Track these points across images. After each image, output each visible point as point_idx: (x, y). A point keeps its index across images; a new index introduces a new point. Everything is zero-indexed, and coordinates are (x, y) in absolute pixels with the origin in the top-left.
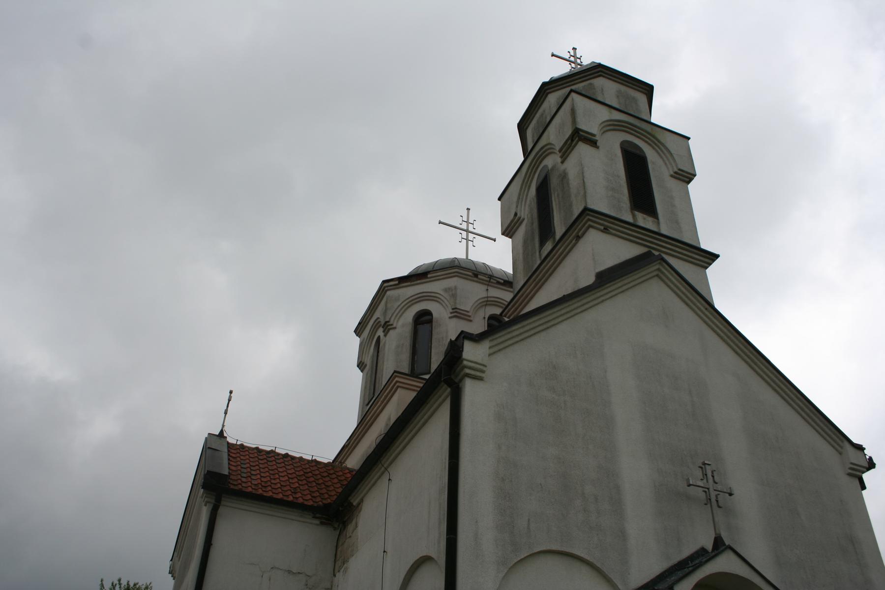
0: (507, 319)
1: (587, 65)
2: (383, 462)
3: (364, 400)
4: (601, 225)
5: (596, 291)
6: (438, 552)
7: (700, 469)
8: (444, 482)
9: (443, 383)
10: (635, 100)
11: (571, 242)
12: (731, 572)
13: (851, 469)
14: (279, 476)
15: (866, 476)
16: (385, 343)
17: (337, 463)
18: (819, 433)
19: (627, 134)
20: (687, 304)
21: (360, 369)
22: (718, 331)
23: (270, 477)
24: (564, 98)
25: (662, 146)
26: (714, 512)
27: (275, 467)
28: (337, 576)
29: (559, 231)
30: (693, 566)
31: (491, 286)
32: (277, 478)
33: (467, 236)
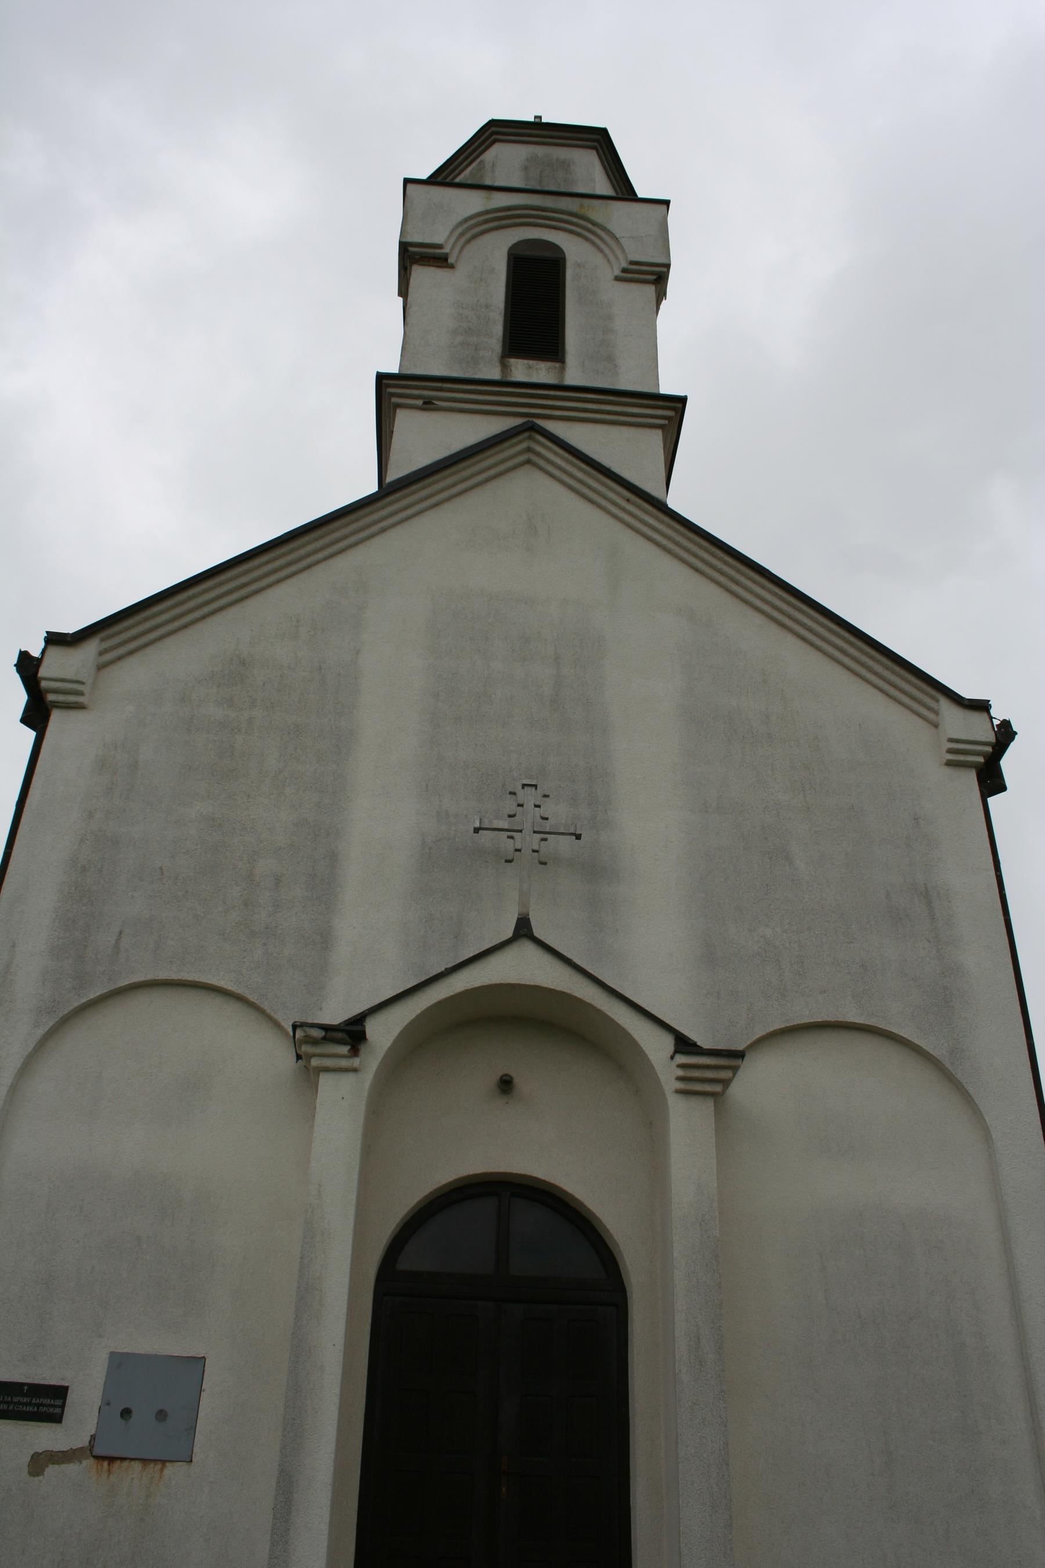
4: (418, 397)
12: (523, 982)
13: (950, 751)
19: (526, 229)
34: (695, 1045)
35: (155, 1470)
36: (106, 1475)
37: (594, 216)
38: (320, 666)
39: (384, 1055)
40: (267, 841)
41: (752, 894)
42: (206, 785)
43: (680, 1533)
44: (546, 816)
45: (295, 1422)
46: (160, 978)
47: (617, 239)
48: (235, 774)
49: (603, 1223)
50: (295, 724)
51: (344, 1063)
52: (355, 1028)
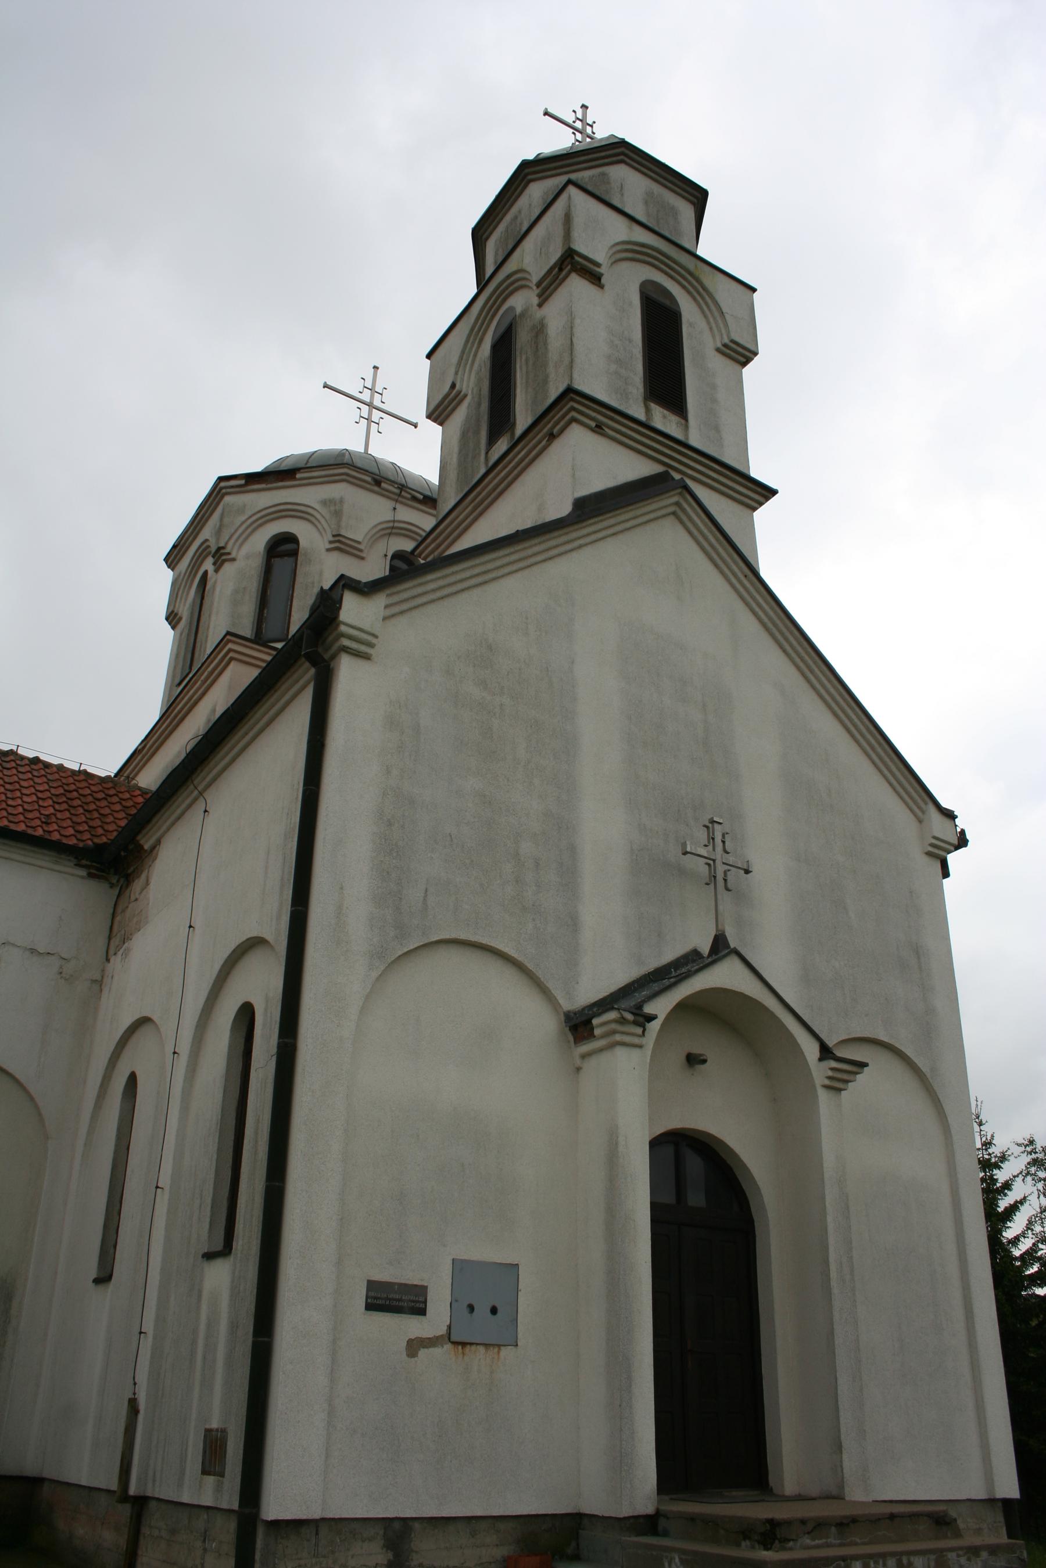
0: (422, 562)
1: (601, 140)
2: (196, 782)
3: (174, 676)
5: (571, 528)
6: (278, 934)
7: (705, 829)
8: (292, 822)
9: (303, 659)
10: (674, 212)
11: (540, 442)
13: (932, 845)
14: (22, 794)
15: (953, 859)
16: (215, 582)
17: (122, 778)
18: (894, 789)
19: (653, 270)
20: (716, 566)
21: (170, 624)
22: (760, 613)
23: (5, 794)
24: (555, 193)
25: (708, 295)
26: (719, 897)
27: (16, 778)
28: (111, 960)
29: (522, 422)
30: (677, 976)
31: (402, 503)
32: (18, 797)
33: (370, 413)
36: (461, 1356)
37: (707, 282)
38: (547, 668)
40: (525, 825)
47: (722, 313)
51: (636, 1040)
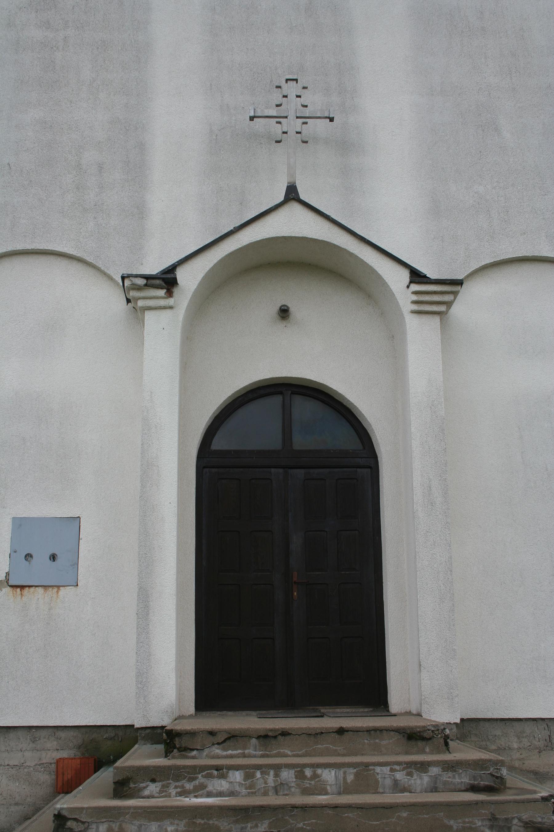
12: (293, 235)
34: (425, 276)
35: (53, 592)
36: (20, 597)
39: (192, 295)
41: (469, 160)
42: (36, 95)
43: (418, 616)
44: (306, 104)
45: (147, 556)
46: (18, 249)
48: (58, 85)
49: (359, 410)
50: (101, 40)
51: (162, 303)
52: (169, 276)
